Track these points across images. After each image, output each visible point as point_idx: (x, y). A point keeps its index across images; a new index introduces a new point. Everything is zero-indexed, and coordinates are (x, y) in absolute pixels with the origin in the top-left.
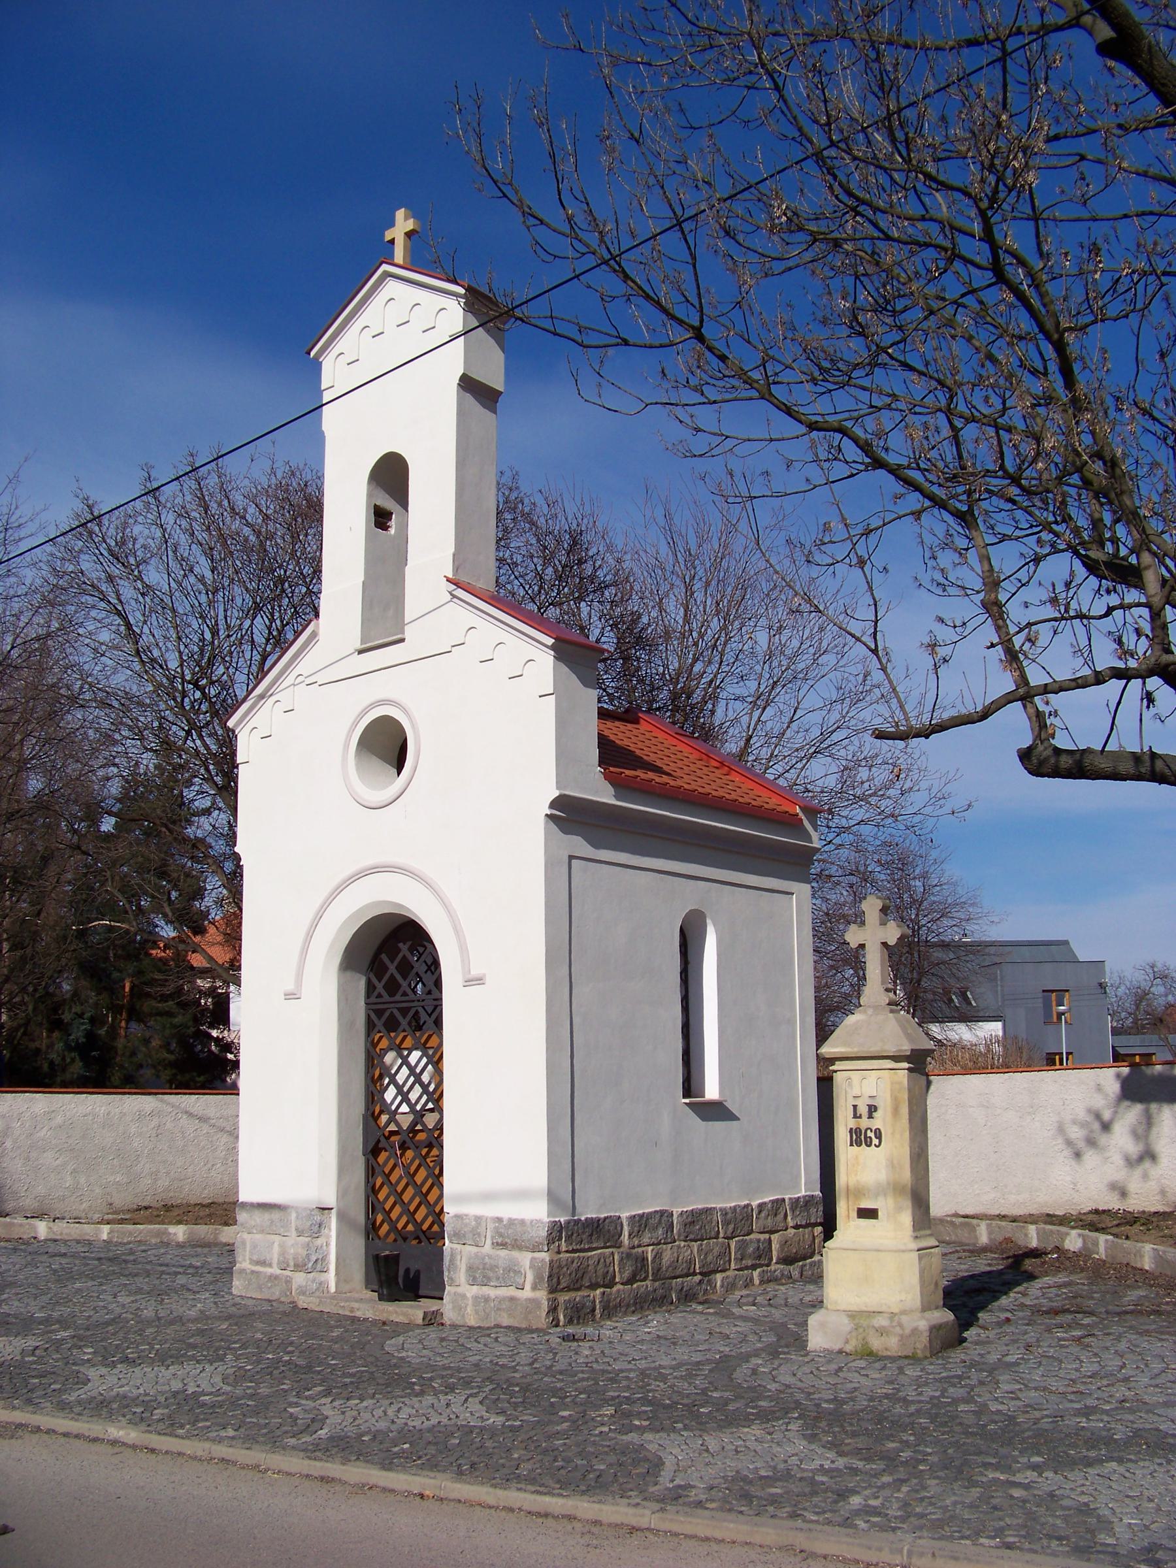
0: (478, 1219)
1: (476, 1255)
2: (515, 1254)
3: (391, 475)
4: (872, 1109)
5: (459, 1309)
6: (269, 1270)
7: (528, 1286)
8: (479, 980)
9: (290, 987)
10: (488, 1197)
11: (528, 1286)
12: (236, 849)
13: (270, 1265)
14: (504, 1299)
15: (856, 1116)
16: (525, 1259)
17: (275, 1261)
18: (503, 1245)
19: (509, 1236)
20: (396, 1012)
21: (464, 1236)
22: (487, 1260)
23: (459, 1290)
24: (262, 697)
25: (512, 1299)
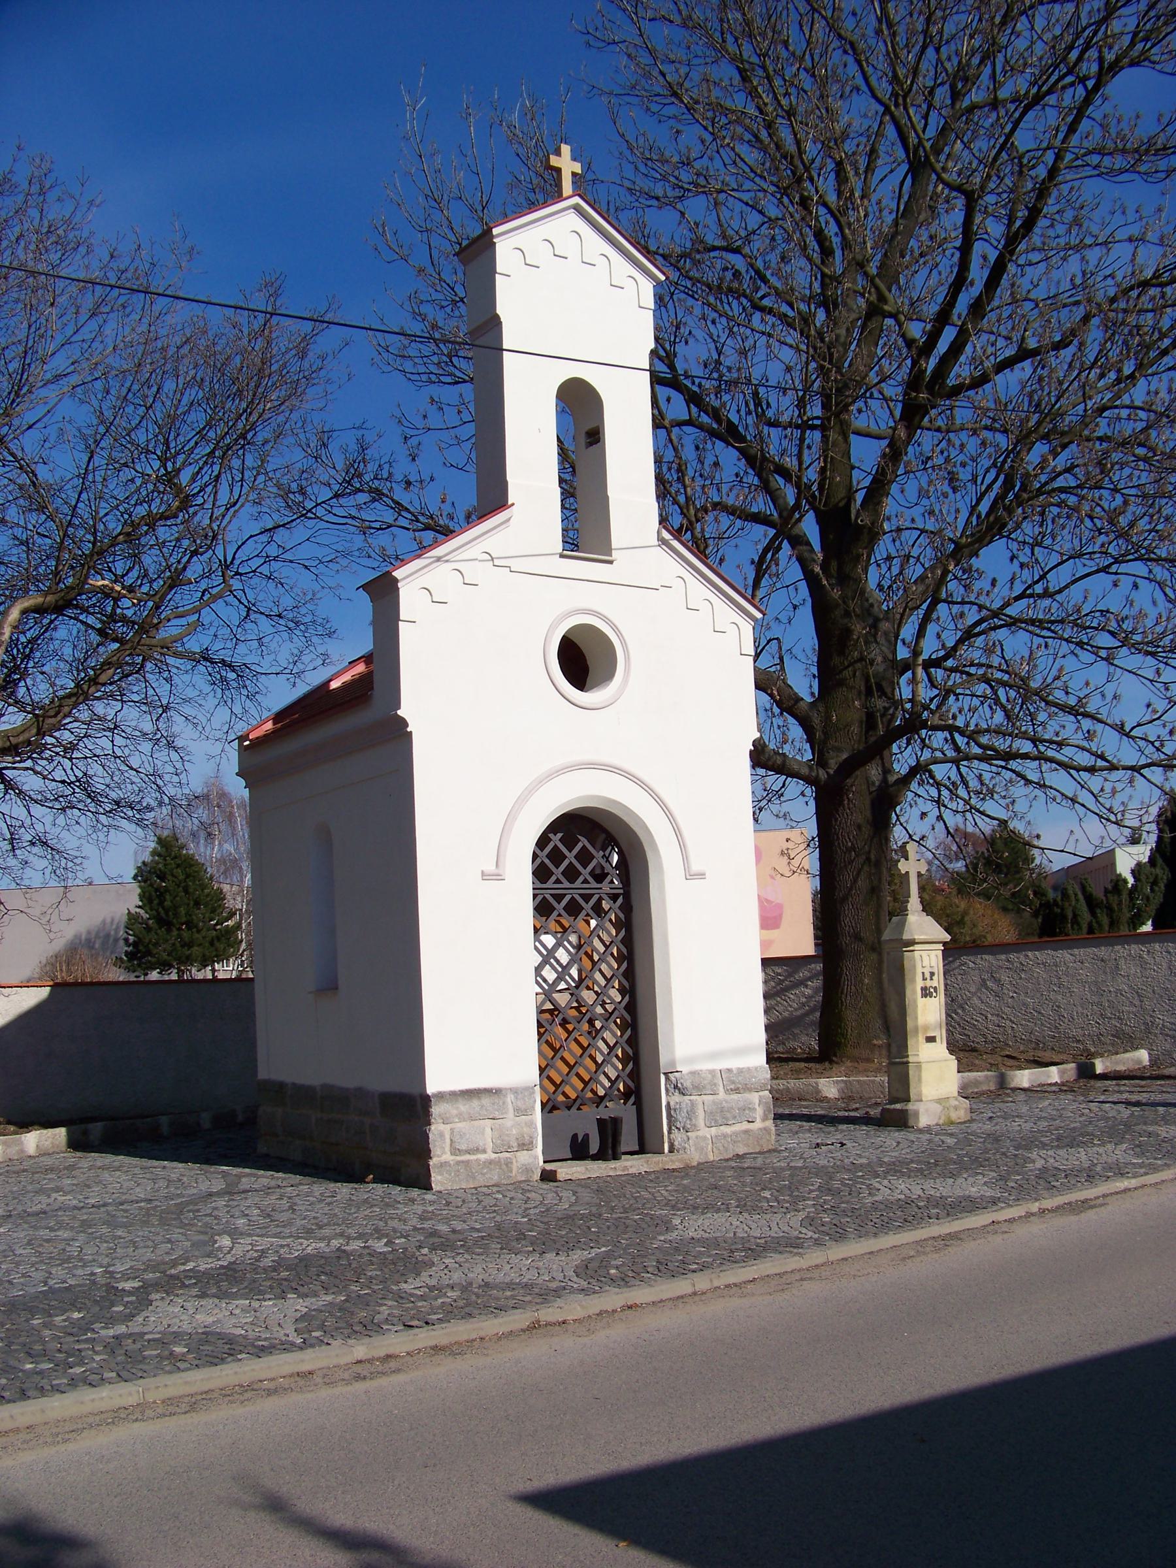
0: (712, 1072)
1: (713, 1102)
2: (747, 1095)
3: (579, 408)
4: (932, 974)
5: (701, 1150)
6: (482, 1157)
7: (758, 1120)
8: (701, 875)
9: (491, 868)
10: (714, 1056)
11: (758, 1120)
12: (758, 735)
13: (484, 1151)
14: (736, 1134)
15: (924, 979)
16: (755, 1097)
17: (490, 1146)
18: (737, 1091)
19: (738, 1083)
20: (577, 897)
21: (704, 1087)
22: (724, 1104)
23: (700, 1133)
24: (439, 559)
25: (746, 1132)
